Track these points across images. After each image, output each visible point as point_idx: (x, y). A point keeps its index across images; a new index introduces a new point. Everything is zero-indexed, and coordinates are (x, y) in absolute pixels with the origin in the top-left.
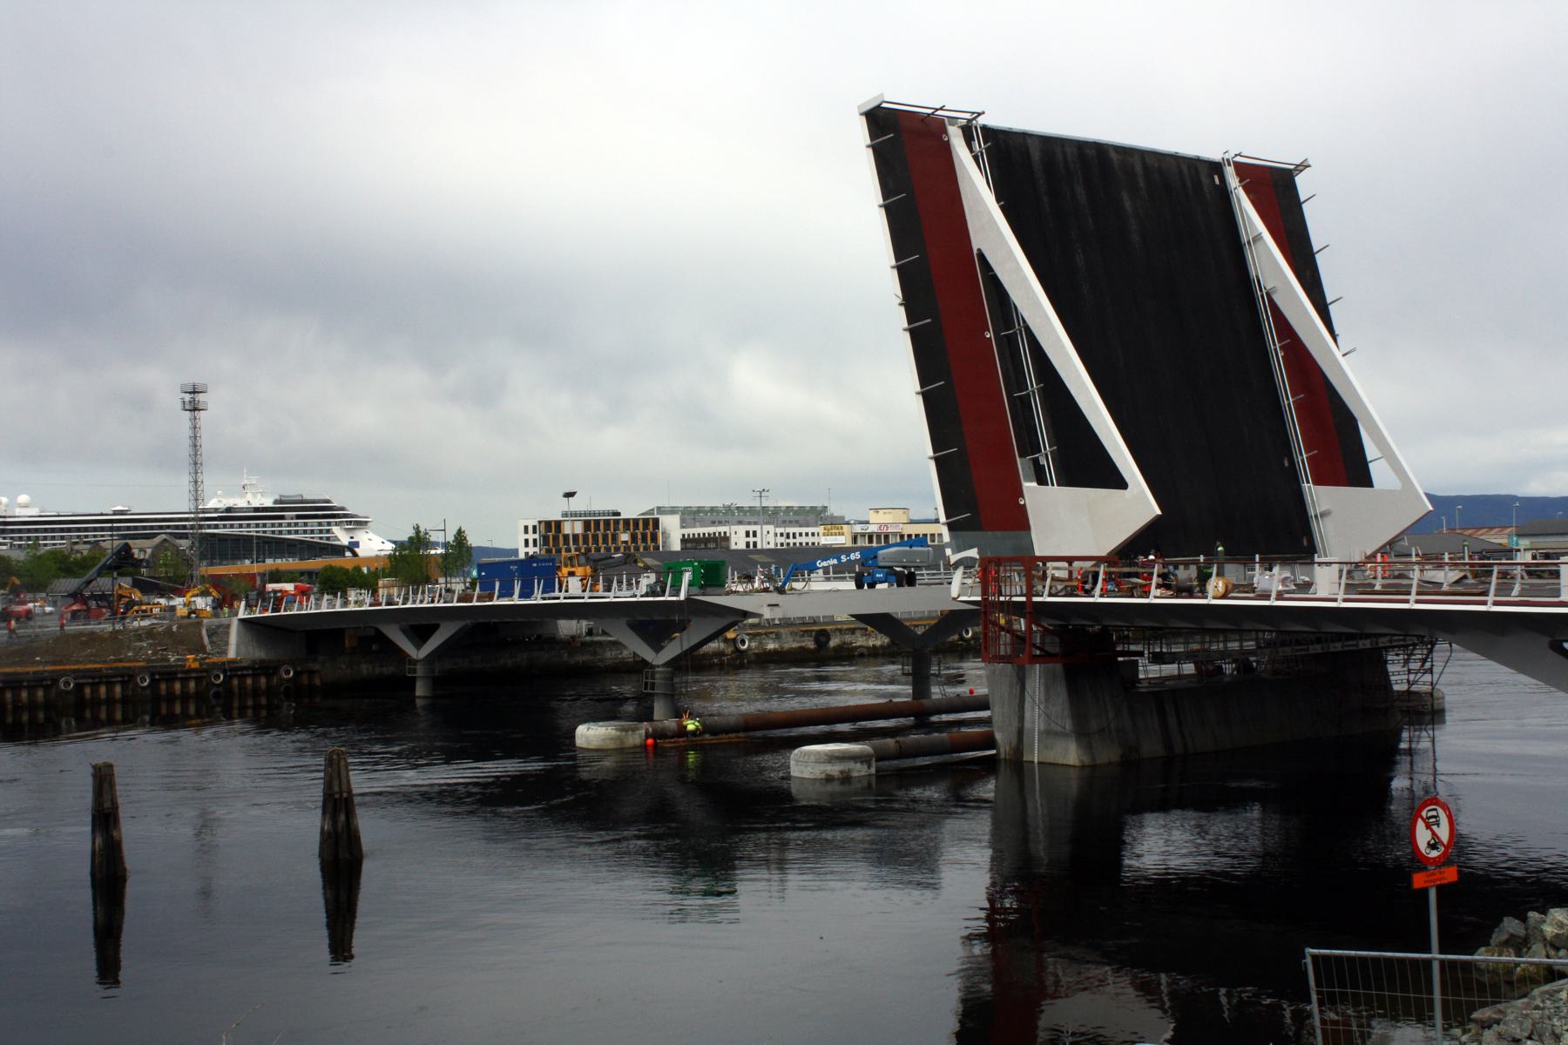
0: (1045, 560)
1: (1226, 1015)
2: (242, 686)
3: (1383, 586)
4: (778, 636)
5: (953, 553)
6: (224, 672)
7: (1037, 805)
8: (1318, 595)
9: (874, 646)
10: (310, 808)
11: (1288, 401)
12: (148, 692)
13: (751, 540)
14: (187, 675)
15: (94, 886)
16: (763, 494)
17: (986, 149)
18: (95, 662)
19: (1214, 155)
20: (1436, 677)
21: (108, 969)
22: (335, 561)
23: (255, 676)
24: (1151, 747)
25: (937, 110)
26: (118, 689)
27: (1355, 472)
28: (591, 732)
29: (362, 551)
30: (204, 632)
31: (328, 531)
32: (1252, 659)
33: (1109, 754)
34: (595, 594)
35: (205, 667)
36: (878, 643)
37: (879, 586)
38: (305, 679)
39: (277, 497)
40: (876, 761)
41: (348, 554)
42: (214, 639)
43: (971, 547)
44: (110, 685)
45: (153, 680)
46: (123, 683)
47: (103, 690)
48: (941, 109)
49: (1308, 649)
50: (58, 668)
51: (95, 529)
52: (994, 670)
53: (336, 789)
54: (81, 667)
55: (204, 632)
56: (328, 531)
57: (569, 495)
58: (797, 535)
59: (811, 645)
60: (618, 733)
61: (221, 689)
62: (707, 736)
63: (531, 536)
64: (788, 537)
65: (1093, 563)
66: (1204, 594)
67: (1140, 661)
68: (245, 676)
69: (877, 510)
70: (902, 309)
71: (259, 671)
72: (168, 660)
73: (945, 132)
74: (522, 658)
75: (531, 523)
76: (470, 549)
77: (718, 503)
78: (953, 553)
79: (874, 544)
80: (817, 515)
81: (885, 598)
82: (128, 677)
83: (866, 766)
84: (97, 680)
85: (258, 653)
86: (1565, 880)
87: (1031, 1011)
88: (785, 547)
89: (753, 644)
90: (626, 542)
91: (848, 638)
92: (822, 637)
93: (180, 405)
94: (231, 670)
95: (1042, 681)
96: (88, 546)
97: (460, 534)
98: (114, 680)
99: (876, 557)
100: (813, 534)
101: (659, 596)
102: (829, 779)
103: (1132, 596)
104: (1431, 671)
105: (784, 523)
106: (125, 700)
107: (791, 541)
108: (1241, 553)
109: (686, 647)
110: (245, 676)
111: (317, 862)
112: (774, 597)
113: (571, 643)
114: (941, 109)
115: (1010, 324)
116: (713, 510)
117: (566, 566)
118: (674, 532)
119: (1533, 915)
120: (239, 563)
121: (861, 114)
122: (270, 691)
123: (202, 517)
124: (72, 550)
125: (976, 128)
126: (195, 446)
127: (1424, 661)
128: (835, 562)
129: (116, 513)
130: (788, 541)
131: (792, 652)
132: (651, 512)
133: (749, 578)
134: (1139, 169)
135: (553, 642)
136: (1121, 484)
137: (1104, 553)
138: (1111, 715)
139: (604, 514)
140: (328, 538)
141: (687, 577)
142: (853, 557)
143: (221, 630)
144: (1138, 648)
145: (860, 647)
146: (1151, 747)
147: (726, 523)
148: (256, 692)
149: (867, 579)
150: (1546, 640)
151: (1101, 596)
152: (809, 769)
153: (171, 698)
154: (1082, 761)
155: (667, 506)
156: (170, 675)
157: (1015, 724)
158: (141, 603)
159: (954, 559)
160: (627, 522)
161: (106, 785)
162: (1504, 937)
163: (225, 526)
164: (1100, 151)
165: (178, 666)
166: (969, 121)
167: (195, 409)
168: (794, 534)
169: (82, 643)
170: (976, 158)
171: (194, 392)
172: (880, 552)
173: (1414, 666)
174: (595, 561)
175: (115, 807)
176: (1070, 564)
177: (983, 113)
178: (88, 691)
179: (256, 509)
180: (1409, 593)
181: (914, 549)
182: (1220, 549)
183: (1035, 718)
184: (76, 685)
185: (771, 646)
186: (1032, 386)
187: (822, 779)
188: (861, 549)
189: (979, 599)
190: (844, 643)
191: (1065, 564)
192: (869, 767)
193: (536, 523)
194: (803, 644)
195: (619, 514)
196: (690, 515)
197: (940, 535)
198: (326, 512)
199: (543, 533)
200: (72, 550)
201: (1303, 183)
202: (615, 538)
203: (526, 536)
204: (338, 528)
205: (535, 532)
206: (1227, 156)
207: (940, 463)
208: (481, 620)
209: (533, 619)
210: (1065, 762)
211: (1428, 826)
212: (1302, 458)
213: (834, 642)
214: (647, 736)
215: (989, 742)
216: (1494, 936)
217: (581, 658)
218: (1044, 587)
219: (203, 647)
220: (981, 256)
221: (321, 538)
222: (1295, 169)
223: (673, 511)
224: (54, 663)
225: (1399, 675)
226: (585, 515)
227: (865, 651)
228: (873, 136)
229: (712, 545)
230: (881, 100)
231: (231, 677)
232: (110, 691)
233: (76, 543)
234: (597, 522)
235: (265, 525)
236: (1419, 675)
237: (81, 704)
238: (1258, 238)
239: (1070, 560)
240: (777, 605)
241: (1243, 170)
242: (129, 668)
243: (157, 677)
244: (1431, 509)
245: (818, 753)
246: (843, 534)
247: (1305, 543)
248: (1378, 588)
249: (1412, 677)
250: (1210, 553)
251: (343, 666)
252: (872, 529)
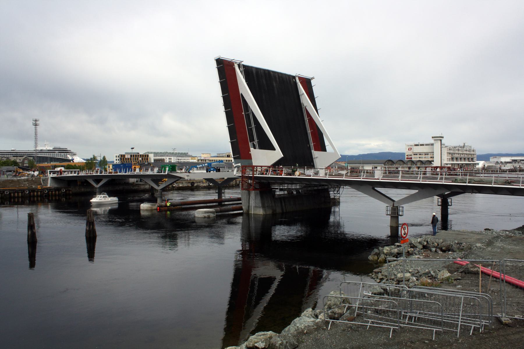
0: (257, 166)
1: (298, 271)
2: (52, 194)
3: (335, 174)
4: (182, 183)
5: (235, 164)
6: (48, 190)
7: (253, 224)
8: (320, 176)
9: (205, 186)
11: (309, 131)
12: (28, 195)
13: (170, 160)
14: (38, 191)
15: (28, 243)
16: (175, 149)
17: (244, 70)
18: (13, 187)
19: (294, 75)
20: (340, 195)
21: (32, 264)
22: (69, 163)
23: (55, 191)
24: (279, 210)
25: (232, 60)
26: (20, 194)
27: (322, 148)
28: (144, 206)
29: (75, 161)
30: (41, 180)
31: (66, 156)
32: (300, 190)
33: (269, 212)
34: (143, 172)
35: (42, 189)
36: (206, 185)
37: (211, 172)
38: (68, 192)
39: (54, 147)
41: (72, 162)
42: (44, 182)
43: (239, 163)
44: (18, 193)
45: (29, 192)
46: (22, 193)
47: (16, 194)
48: (234, 60)
49: (314, 188)
50: (4, 188)
51: (6, 154)
52: (243, 192)
53: (90, 219)
54: (11, 188)
55: (41, 180)
56: (66, 156)
57: (132, 148)
59: (190, 185)
60: (151, 206)
61: (47, 194)
62: (172, 207)
63: (117, 158)
65: (267, 167)
66: (282, 175)
67: (277, 190)
68: (53, 191)
69: (203, 154)
70: (224, 106)
71: (56, 190)
72: (32, 187)
73: (234, 65)
74: (121, 187)
75: (117, 155)
76: (106, 161)
77: (163, 151)
78: (235, 164)
80: (186, 155)
81: (213, 175)
82: (23, 191)
83: (213, 214)
84: (15, 192)
85: (55, 186)
87: (250, 271)
89: (176, 185)
90: (140, 160)
91: (199, 184)
92: (193, 183)
93: (32, 124)
94: (49, 190)
95: (254, 195)
96: (6, 158)
97: (104, 158)
98: (19, 192)
99: (211, 165)
100: (185, 159)
101: (160, 173)
102: (205, 217)
103: (277, 175)
104: (339, 193)
105: (178, 156)
106: (22, 197)
107: (179, 161)
108: (302, 166)
109: (167, 185)
110: (53, 191)
111: (85, 237)
112: (188, 174)
113: (133, 184)
114: (234, 60)
115: (248, 111)
116: (161, 153)
117: (134, 165)
118: (152, 158)
119: (380, 248)
120: (44, 163)
121: (215, 60)
122: (59, 195)
123: (37, 152)
124: (1, 159)
125: (241, 65)
126: (36, 134)
127: (338, 191)
128: (201, 166)
129: (12, 150)
131: (186, 187)
132: (146, 153)
133: (182, 169)
134: (277, 77)
135: (128, 184)
136: (274, 149)
137: (270, 165)
138: (270, 203)
139: (135, 153)
140: (66, 158)
141: (167, 169)
142: (206, 165)
143: (46, 180)
144: (277, 187)
145: (202, 186)
146: (279, 210)
147: (164, 156)
148: (55, 195)
149: (209, 170)
150: (371, 187)
151: (270, 175)
152: (200, 215)
153: (34, 196)
154: (263, 213)
156: (33, 191)
157: (248, 204)
158: (22, 173)
159: (235, 166)
160: (141, 155)
161: (31, 218)
162: (374, 253)
163: (40, 154)
164: (269, 71)
165: (36, 188)
166: (240, 63)
167: (36, 125)
168: (180, 159)
169: (10, 182)
170: (241, 72)
171: (36, 121)
172: (212, 164)
173: (335, 192)
174: (141, 164)
175: (34, 224)
176: (262, 168)
177: (243, 61)
178: (12, 194)
179: (48, 150)
180: (343, 176)
181: (220, 163)
182: (297, 165)
183: (252, 203)
184: (9, 193)
185: (181, 185)
186: (253, 126)
187: (203, 217)
188: (208, 163)
189: (241, 175)
190: (198, 185)
191: (260, 168)
192: (214, 214)
193: (119, 155)
194: (188, 185)
195: (139, 153)
196: (156, 154)
197: (231, 160)
198: (66, 151)
199: (120, 157)
200: (1, 159)
201: (313, 82)
202: (138, 159)
203: (116, 158)
204: (69, 155)
205: (118, 157)
206: (296, 75)
207: (232, 143)
208: (113, 178)
209: (123, 178)
210: (259, 214)
211: (404, 230)
212: (312, 145)
213: (195, 185)
214: (158, 207)
215: (241, 209)
216: (372, 253)
217: (136, 188)
218: (257, 173)
219: (41, 184)
220: (242, 95)
221: (64, 158)
222: (311, 79)
223: (151, 153)
224: (3, 187)
225: (332, 194)
226: (131, 153)
227: (203, 187)
228: (217, 65)
229: (160, 161)
230: (219, 57)
231: (49, 191)
232: (18, 194)
233: (3, 158)
234: (134, 155)
235: (50, 154)
236: (337, 194)
237: (11, 197)
238: (303, 94)
239: (261, 167)
240: (189, 176)
241: (300, 78)
242: (23, 189)
243: (30, 191)
244: (341, 157)
245: (202, 211)
246: (195, 159)
247: (312, 164)
248: (334, 175)
249: (335, 195)
250: (295, 166)
251: (77, 189)
252: (202, 158)
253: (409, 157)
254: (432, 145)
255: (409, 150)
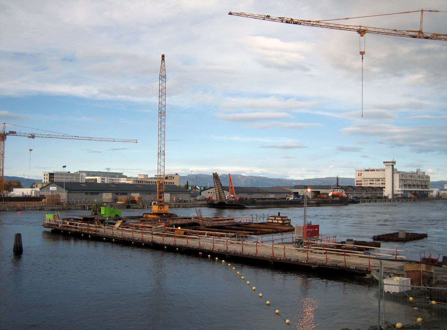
10: (46, 210)
13: (103, 180)
40: (92, 205)
57: (64, 167)
58: (115, 180)
64: (112, 180)
79: (147, 184)
86: (446, 278)
88: (116, 183)
130: (112, 181)
155: (81, 170)
168: (116, 180)
246: (131, 180)
253: (359, 183)
254: (384, 170)
255: (359, 175)
